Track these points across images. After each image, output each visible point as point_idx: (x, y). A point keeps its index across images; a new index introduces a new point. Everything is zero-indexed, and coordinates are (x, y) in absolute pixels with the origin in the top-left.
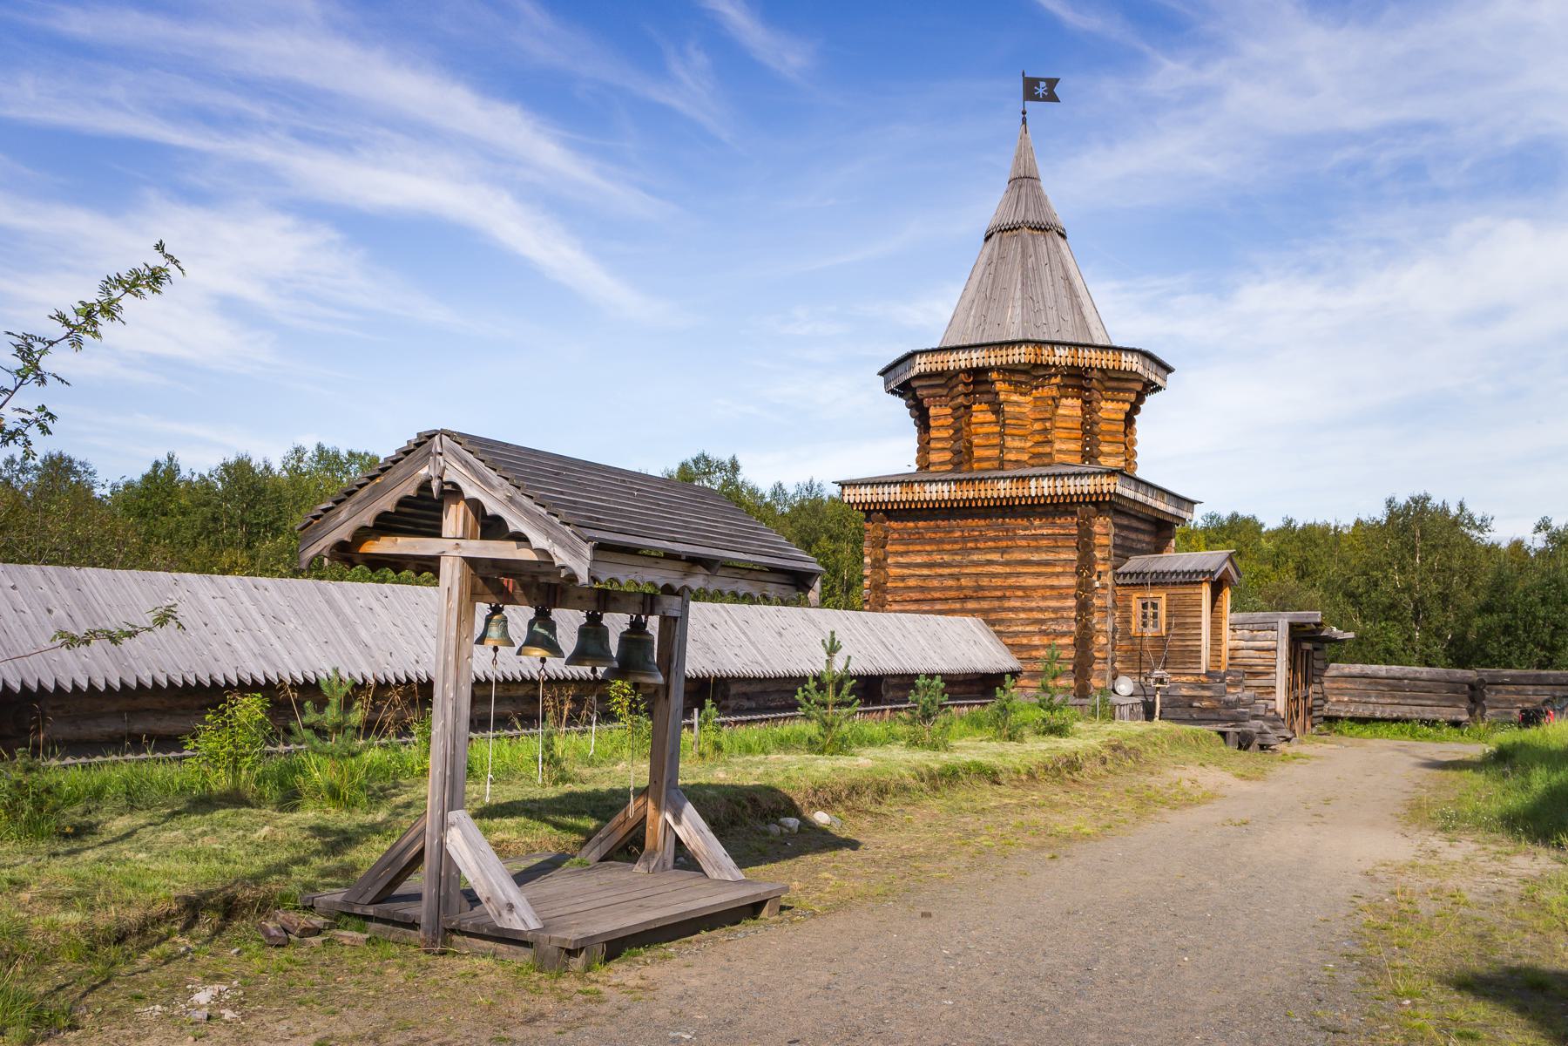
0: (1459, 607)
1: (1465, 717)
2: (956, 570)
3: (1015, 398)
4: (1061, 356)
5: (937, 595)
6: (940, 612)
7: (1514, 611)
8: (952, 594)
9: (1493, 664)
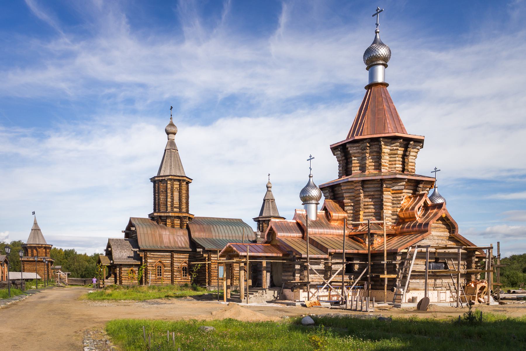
1: (84, 284)
4: (44, 246)
6: (32, 272)
9: (86, 278)
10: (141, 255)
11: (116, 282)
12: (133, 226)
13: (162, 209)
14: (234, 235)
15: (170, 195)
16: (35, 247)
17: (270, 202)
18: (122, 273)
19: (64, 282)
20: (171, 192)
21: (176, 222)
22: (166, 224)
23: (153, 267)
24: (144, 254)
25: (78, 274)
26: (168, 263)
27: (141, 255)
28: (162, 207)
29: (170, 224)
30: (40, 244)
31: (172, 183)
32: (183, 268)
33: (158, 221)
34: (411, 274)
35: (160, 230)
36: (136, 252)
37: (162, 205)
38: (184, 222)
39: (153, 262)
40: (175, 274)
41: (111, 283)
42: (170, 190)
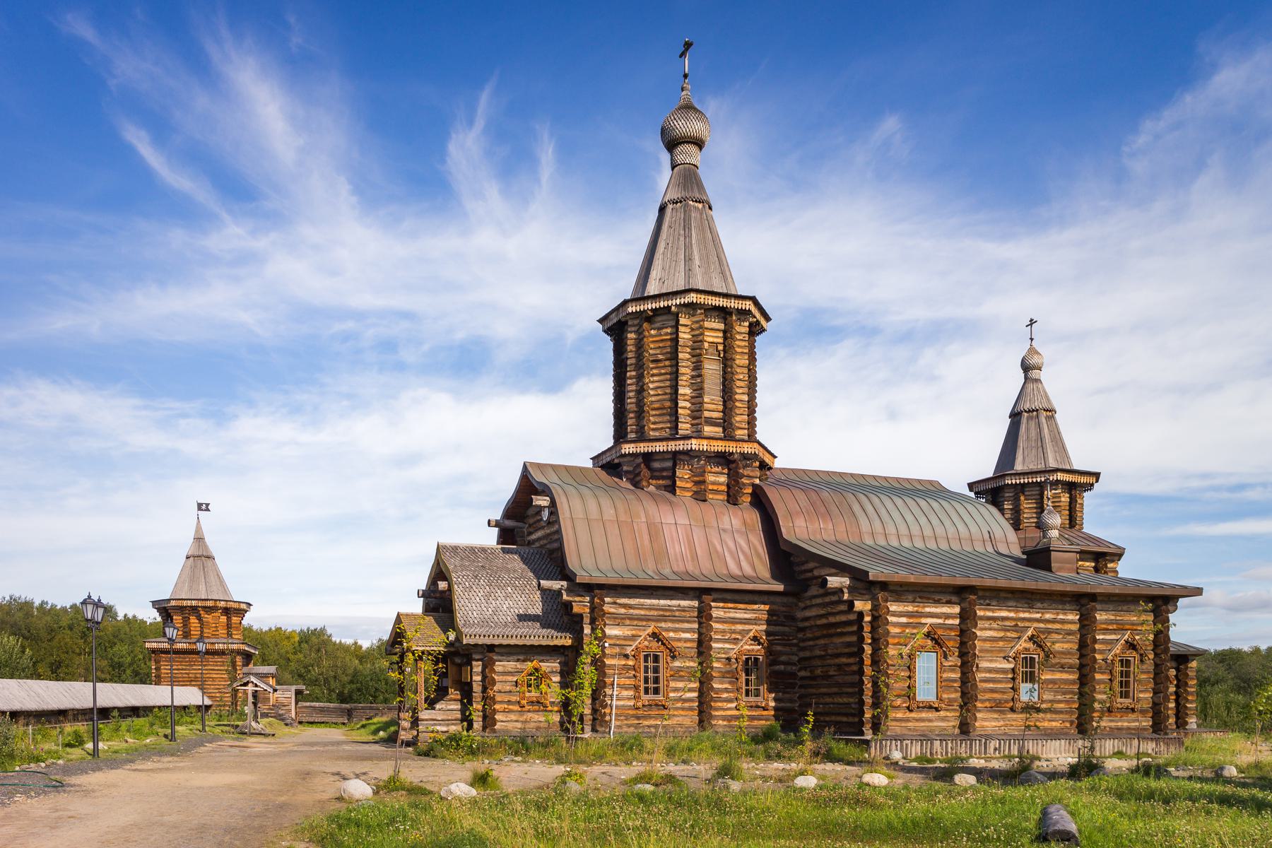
0: (341, 681)
1: (346, 721)
2: (187, 672)
3: (206, 616)
4: (222, 604)
5: (181, 679)
7: (361, 683)
8: (187, 679)
10: (576, 609)
11: (467, 720)
12: (545, 491)
13: (655, 423)
14: (940, 531)
15: (688, 371)
16: (194, 609)
17: (1043, 420)
18: (494, 682)
19: (282, 715)
20: (694, 360)
21: (711, 478)
22: (672, 489)
23: (626, 656)
24: (592, 602)
25: (331, 691)
26: (687, 640)
27: (576, 609)
28: (654, 423)
29: (689, 485)
30: (210, 600)
31: (697, 322)
32: (747, 660)
33: (639, 474)
34: (654, 694)
35: (651, 507)
36: (559, 593)
37: (653, 416)
38: (745, 481)
39: (625, 638)
40: (715, 686)
41: (448, 725)
42: (689, 350)
